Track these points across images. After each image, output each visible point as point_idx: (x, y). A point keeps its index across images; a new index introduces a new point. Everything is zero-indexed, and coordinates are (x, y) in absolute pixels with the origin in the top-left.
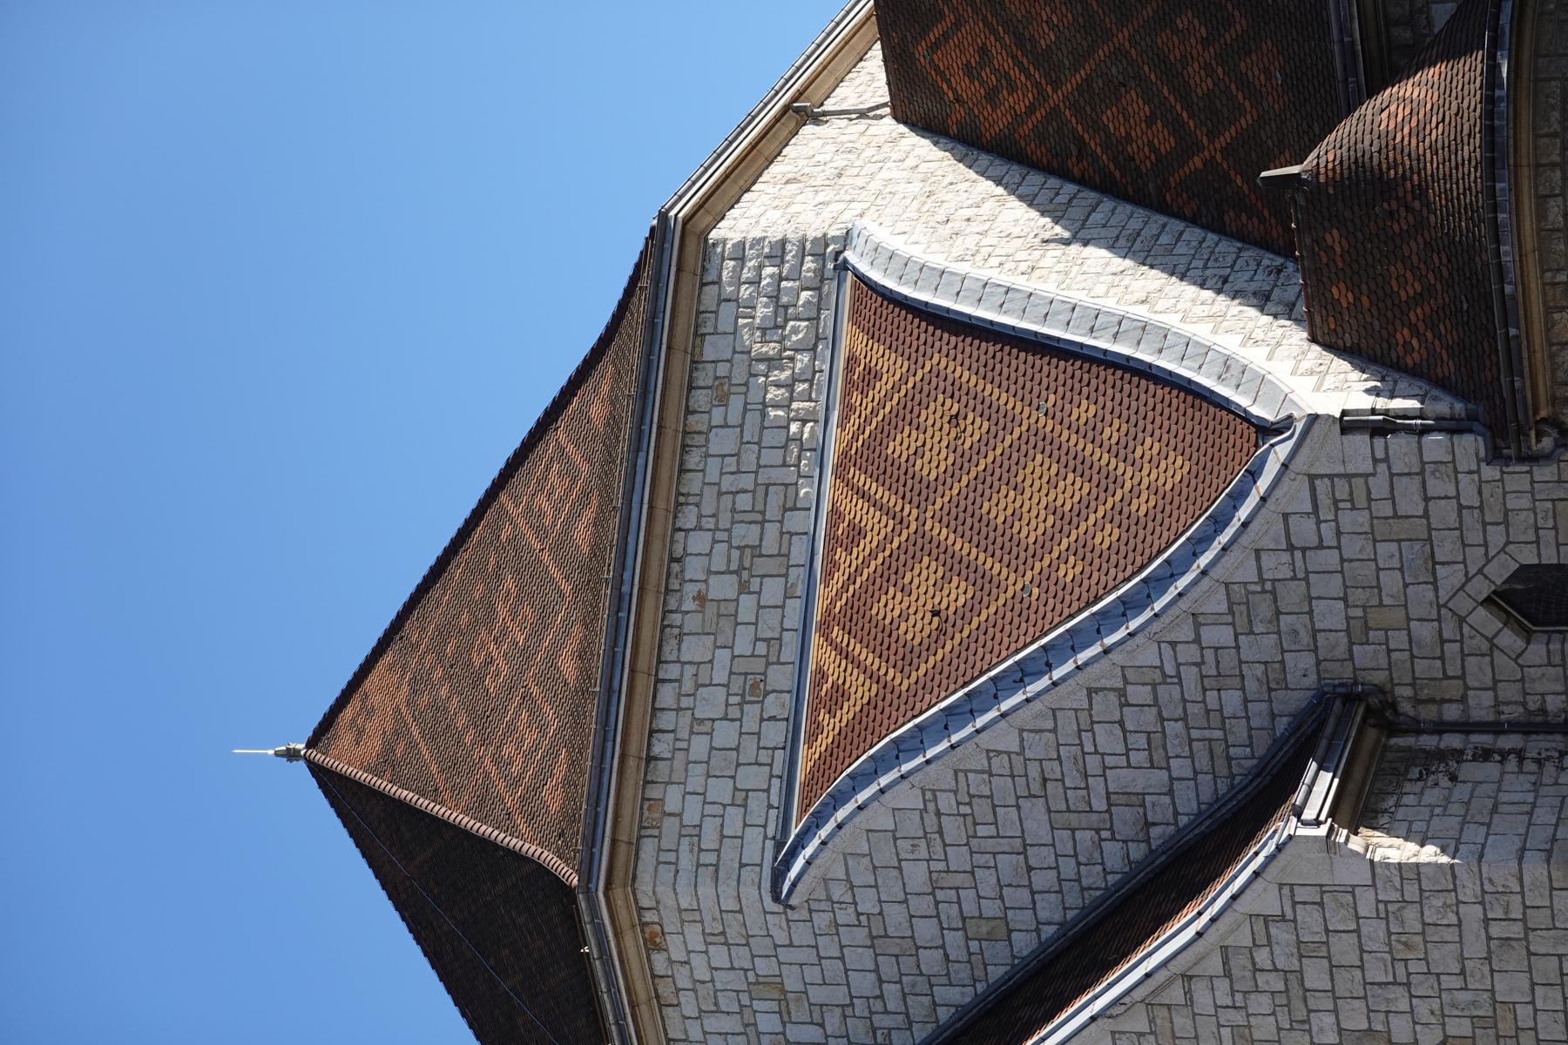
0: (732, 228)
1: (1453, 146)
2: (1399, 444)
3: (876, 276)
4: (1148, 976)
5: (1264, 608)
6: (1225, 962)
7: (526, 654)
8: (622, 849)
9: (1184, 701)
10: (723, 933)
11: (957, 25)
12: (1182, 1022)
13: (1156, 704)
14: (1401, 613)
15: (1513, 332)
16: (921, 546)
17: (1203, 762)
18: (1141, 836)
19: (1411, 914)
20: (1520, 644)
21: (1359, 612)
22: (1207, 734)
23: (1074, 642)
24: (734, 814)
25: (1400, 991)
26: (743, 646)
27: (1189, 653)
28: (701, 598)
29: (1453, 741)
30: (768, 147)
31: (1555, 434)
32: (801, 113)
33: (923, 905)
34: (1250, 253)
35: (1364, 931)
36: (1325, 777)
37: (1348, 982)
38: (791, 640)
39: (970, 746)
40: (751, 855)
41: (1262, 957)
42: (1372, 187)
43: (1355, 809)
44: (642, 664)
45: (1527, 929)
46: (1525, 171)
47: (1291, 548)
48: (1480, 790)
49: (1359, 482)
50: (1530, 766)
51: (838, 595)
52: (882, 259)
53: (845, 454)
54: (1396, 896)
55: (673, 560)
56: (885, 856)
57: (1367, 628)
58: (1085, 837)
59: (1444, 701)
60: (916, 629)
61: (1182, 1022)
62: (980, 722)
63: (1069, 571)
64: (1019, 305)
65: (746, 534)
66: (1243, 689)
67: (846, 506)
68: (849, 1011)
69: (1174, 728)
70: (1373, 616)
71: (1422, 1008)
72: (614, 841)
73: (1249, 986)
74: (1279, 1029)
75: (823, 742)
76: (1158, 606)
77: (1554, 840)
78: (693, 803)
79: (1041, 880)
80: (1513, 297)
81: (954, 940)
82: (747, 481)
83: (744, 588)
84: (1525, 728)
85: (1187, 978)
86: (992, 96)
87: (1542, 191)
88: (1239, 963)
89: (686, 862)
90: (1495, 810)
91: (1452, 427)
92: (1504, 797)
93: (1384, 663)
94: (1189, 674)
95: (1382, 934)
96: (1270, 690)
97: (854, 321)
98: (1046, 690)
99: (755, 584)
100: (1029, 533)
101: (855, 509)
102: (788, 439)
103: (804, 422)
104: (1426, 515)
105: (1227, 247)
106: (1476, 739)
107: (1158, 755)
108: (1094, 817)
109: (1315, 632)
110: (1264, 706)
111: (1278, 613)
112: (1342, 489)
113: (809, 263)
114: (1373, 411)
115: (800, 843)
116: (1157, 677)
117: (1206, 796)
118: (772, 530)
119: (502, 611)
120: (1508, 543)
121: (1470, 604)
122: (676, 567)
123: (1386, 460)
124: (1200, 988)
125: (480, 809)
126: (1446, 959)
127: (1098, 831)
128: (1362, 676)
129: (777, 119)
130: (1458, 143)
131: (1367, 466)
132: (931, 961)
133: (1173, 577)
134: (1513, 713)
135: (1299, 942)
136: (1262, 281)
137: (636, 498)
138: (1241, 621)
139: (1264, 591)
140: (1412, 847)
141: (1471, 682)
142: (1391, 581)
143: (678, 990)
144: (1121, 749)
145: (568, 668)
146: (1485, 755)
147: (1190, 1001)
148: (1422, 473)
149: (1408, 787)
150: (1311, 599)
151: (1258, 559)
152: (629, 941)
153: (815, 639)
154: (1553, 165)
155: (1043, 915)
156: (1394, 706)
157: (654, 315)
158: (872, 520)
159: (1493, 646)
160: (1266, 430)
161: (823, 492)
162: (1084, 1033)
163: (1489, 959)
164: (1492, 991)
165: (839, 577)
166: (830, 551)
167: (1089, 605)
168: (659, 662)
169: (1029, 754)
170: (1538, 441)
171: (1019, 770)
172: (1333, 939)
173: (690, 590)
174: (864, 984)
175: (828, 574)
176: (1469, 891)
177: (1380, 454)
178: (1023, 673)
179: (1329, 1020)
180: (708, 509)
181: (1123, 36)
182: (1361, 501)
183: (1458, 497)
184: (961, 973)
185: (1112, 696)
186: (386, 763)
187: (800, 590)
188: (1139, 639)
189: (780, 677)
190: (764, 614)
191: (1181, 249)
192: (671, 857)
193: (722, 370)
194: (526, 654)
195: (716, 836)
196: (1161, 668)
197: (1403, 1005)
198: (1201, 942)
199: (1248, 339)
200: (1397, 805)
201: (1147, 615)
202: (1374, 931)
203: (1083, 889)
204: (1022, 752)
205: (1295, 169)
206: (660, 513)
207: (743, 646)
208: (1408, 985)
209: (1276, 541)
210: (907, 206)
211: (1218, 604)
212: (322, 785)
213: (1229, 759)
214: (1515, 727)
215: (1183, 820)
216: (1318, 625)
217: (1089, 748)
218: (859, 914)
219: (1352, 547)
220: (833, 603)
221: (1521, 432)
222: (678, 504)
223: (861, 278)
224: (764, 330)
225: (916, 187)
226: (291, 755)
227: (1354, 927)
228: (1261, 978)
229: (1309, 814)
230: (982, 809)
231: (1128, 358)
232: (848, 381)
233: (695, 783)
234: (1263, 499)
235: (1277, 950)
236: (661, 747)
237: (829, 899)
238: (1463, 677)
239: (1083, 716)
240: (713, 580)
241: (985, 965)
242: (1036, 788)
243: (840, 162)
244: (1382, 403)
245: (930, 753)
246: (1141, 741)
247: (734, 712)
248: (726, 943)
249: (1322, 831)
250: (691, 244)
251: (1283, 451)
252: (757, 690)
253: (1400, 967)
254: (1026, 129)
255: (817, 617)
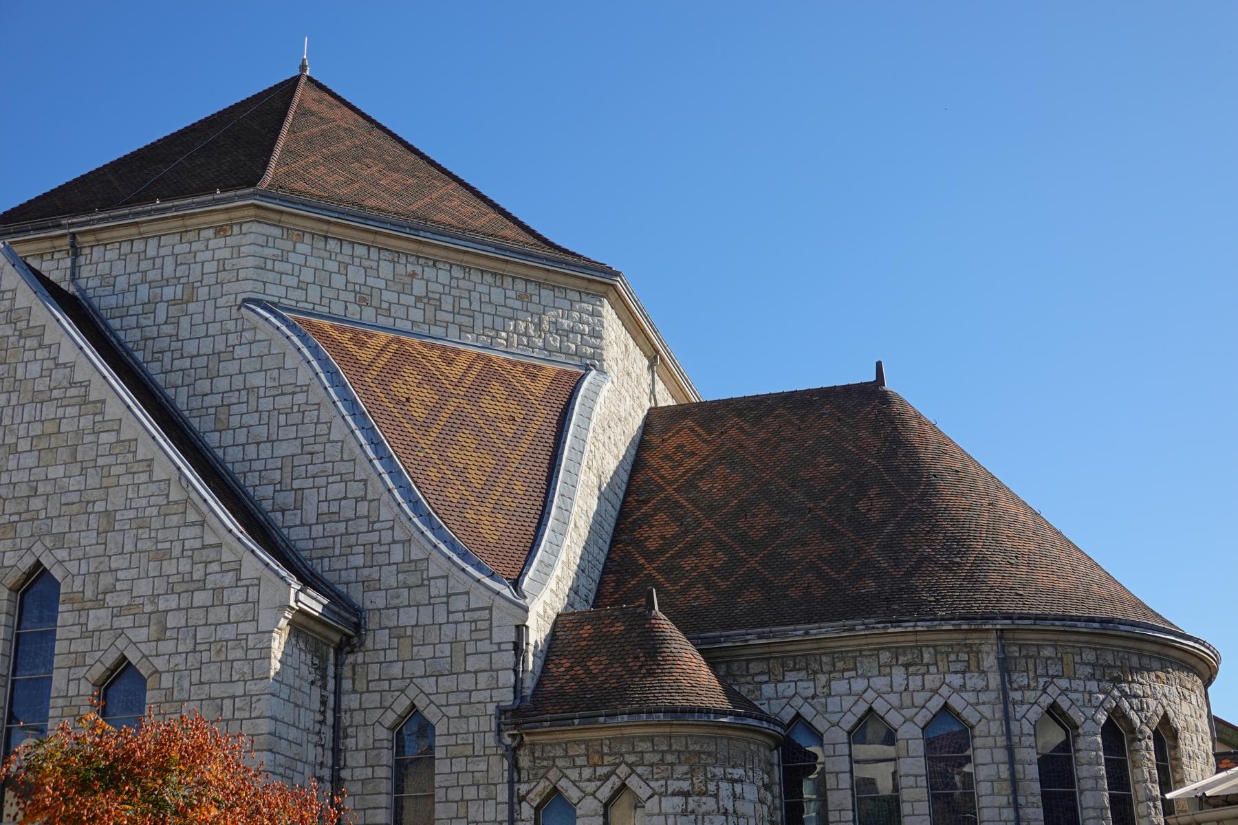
0: (608, 312)
1: (679, 690)
2: (509, 657)
3: (585, 384)
4: (205, 501)
5: (412, 579)
6: (211, 546)
7: (376, 184)
8: (277, 217)
9: (358, 534)
10: (224, 270)
11: (705, 441)
12: (175, 520)
13: (357, 518)
14: (407, 656)
15: (576, 721)
16: (444, 396)
17: (321, 543)
18: (276, 507)
19: (239, 653)
20: (388, 724)
21: (409, 633)
22: (338, 546)
23: (395, 473)
24: (293, 281)
25: (191, 647)
26: (389, 296)
27: (387, 537)
28: (413, 275)
29: (331, 685)
30: (641, 338)
31: (514, 744)
32: (654, 358)
33: (238, 382)
34: (594, 586)
35: (229, 626)
36: (319, 608)
37: (197, 616)
38: (389, 322)
39: (335, 412)
40: (271, 289)
41: (215, 567)
42: (651, 648)
43: (301, 626)
44: (380, 239)
45: (228, 721)
46: (667, 730)
47: (448, 596)
48: (306, 697)
49: (487, 634)
50: (318, 727)
51: (415, 349)
52: (594, 388)
53: (490, 360)
54: (251, 644)
55: (435, 262)
56: (269, 363)
57: (399, 638)
58: (277, 475)
59: (354, 681)
60: (399, 389)
61: (175, 520)
62: (349, 418)
63: (432, 472)
64: (574, 457)
65: (447, 303)
66: (364, 567)
67: (463, 358)
68: (174, 338)
69: (341, 527)
70: (407, 641)
71: (179, 659)
72: (281, 212)
73: (196, 559)
74: (168, 576)
75: (335, 334)
76: (416, 520)
77: (281, 738)
78: (301, 260)
79: (251, 451)
80: (597, 722)
81: (217, 400)
82: (476, 306)
83: (418, 299)
84: (336, 726)
85: (203, 524)
86: (667, 457)
87: (656, 739)
88: (212, 554)
89: (268, 252)
90: (296, 705)
91: (517, 688)
92: (302, 710)
93: (378, 646)
94: (374, 537)
95: (227, 637)
96: (363, 582)
97: (560, 372)
98: (367, 456)
99: (420, 305)
100: (452, 453)
101: (461, 363)
102: (497, 331)
103: (506, 340)
104: (466, 672)
105: (596, 575)
106: (332, 697)
107: (326, 518)
108: (289, 481)
109: (398, 608)
110: (354, 579)
111: (410, 588)
112: (483, 625)
113: (590, 351)
114: (527, 644)
115: (276, 315)
116: (374, 519)
117: (300, 545)
118: (449, 317)
119: (396, 176)
120: (449, 718)
121: (412, 696)
122: (431, 263)
123: (500, 650)
124: (196, 531)
125: (287, 151)
126: (210, 672)
127: (280, 483)
128: (371, 634)
129: (653, 345)
130: (683, 694)
131: (496, 639)
132: (204, 386)
133: (432, 530)
134: (346, 720)
135: (223, 588)
136: (583, 591)
137: (471, 244)
138: (405, 567)
139: (423, 580)
140: (279, 656)
141: (365, 696)
142: (427, 652)
143: (190, 243)
144: (330, 497)
145: (372, 202)
146: (324, 703)
147: (187, 525)
148: (492, 670)
149: (309, 656)
150: (418, 606)
151: (442, 577)
152: (222, 216)
153: (390, 335)
154: (671, 746)
155: (230, 450)
156: (352, 652)
157: (567, 264)
158: (456, 371)
159: (387, 709)
160: (516, 584)
161: (470, 345)
162: (170, 464)
163: (210, 698)
164: (189, 700)
165: (425, 351)
166: (439, 347)
167: (415, 483)
168: (380, 249)
169: (328, 445)
170: (509, 735)
171: (319, 439)
172: (225, 608)
173: (418, 270)
174: (191, 347)
175: (426, 345)
176: (252, 687)
177: (503, 647)
178: (376, 444)
179: (174, 606)
180: (461, 283)
181: (708, 524)
182: (475, 636)
183: (477, 690)
184: (195, 403)
185: (362, 493)
186: (304, 112)
187: (416, 330)
188: (396, 509)
189: (369, 315)
190: (404, 309)
191: (596, 550)
192: (271, 244)
193: (535, 299)
194: (376, 184)
195: (282, 270)
196: (379, 521)
197: (181, 649)
198: (226, 532)
199: (559, 579)
200: (300, 649)
201: (411, 514)
202: (229, 633)
203: (245, 473)
204: (329, 441)
205: (656, 607)
206: (461, 257)
207: (389, 296)
208: (194, 651)
209: (453, 588)
210: (614, 411)
211: (416, 554)
212: (287, 81)
213: (322, 558)
214: (337, 720)
215: (285, 531)
216: (401, 610)
217: (331, 479)
218: (234, 346)
219: (448, 631)
220: (410, 346)
221: (517, 725)
222: (464, 268)
223: (583, 377)
224: (555, 323)
225: (623, 414)
226: (303, 68)
227: (232, 620)
228: (201, 566)
229: (302, 596)
230: (296, 418)
231: (549, 513)
232: (529, 365)
233: (312, 261)
234: (479, 581)
235: (218, 576)
236: (332, 244)
237: (244, 330)
238: (368, 691)
239: (350, 477)
240: (423, 282)
241: (200, 417)
242: (308, 449)
243: (634, 375)
244: (531, 648)
245: (330, 390)
246: (334, 508)
247: (350, 287)
248: (218, 272)
249: (293, 604)
250: (602, 288)
251: (507, 592)
252: (363, 300)
253: (206, 647)
254: (650, 473)
255: (402, 337)
